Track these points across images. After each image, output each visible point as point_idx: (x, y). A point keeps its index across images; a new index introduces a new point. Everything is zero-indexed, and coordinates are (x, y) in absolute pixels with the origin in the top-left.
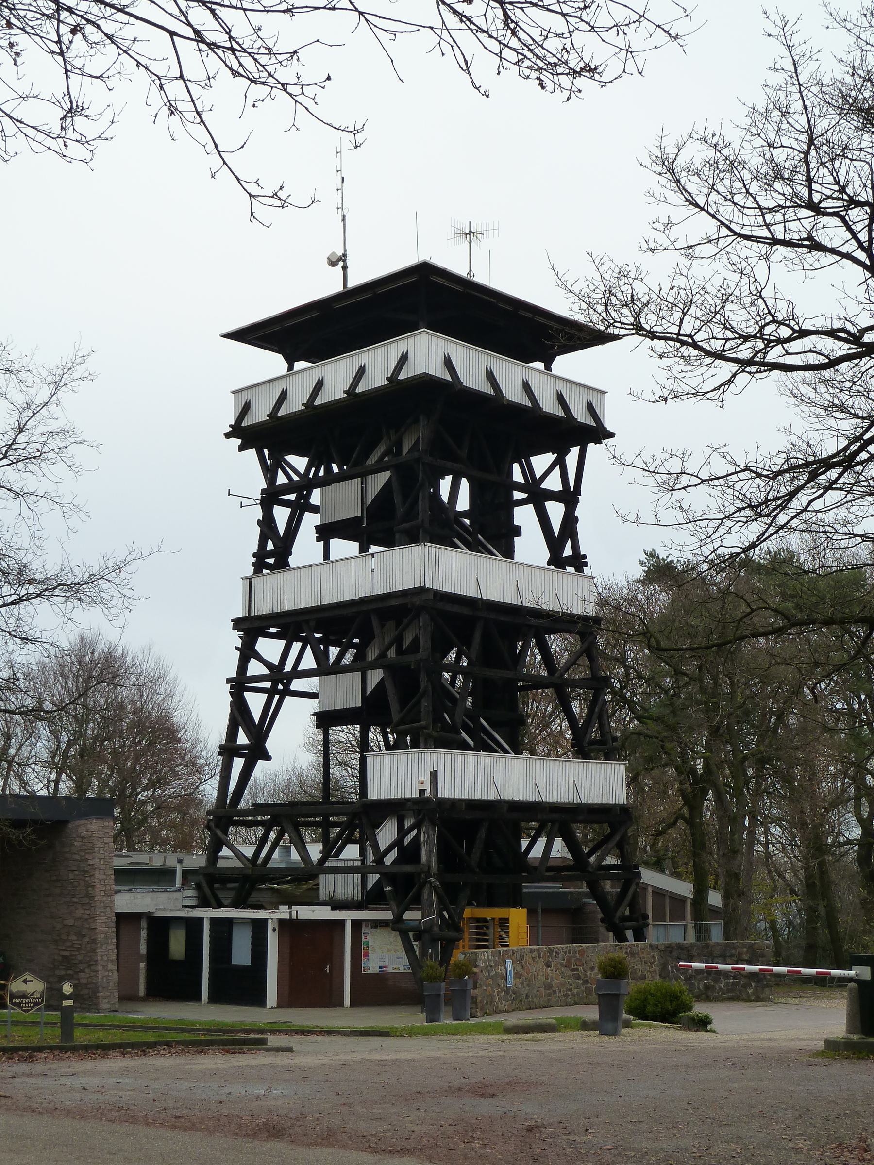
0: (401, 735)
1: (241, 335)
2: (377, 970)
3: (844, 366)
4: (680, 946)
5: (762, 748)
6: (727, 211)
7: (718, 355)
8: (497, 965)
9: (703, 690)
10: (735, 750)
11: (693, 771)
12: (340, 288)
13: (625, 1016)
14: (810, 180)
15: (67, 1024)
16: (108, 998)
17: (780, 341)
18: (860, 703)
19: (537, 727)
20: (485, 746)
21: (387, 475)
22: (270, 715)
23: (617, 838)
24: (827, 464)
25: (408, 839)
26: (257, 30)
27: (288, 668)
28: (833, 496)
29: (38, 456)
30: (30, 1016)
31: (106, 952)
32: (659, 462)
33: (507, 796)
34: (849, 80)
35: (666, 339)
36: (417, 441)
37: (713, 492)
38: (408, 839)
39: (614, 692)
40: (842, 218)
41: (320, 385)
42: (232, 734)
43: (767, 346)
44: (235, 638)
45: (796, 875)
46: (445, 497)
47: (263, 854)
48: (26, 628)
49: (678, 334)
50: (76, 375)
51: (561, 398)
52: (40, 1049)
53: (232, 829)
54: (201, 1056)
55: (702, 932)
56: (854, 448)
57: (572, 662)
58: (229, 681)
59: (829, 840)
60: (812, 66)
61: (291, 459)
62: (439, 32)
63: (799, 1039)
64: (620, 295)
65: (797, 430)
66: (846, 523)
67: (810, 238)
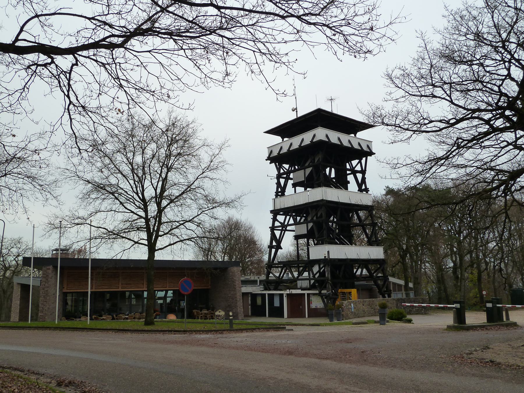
0: (318, 241)
1: (269, 132)
2: (315, 307)
3: (443, 131)
4: (401, 299)
5: (423, 241)
6: (408, 88)
7: (407, 129)
8: (349, 305)
9: (405, 225)
10: (415, 243)
11: (403, 249)
12: (296, 117)
13: (387, 319)
14: (432, 78)
15: (231, 323)
16: (241, 316)
17: (425, 124)
18: (451, 227)
19: (356, 237)
20: (342, 243)
21: (311, 169)
22: (282, 237)
23: (382, 268)
24: (440, 159)
25: (322, 270)
26: (274, 48)
27: (286, 223)
28: (443, 168)
29: (217, 168)
30: (220, 321)
31: (240, 303)
32: (391, 161)
33: (349, 257)
34: (441, 48)
35: (391, 126)
36: (319, 158)
37: (407, 169)
38: (322, 270)
39: (378, 227)
40: (442, 88)
41: (291, 144)
42: (271, 242)
43: (421, 126)
44: (271, 216)
45: (434, 278)
46: (328, 174)
47: (281, 276)
48: (215, 215)
49: (395, 124)
50: (226, 146)
51: (359, 144)
52: (224, 330)
53: (272, 269)
54: (268, 332)
55: (407, 295)
56: (448, 154)
57: (366, 219)
58: (270, 228)
59: (444, 267)
60: (430, 45)
61: (284, 165)
62: (327, 45)
63: (439, 325)
64: (377, 114)
65: (431, 149)
66: (446, 176)
67: (432, 94)
